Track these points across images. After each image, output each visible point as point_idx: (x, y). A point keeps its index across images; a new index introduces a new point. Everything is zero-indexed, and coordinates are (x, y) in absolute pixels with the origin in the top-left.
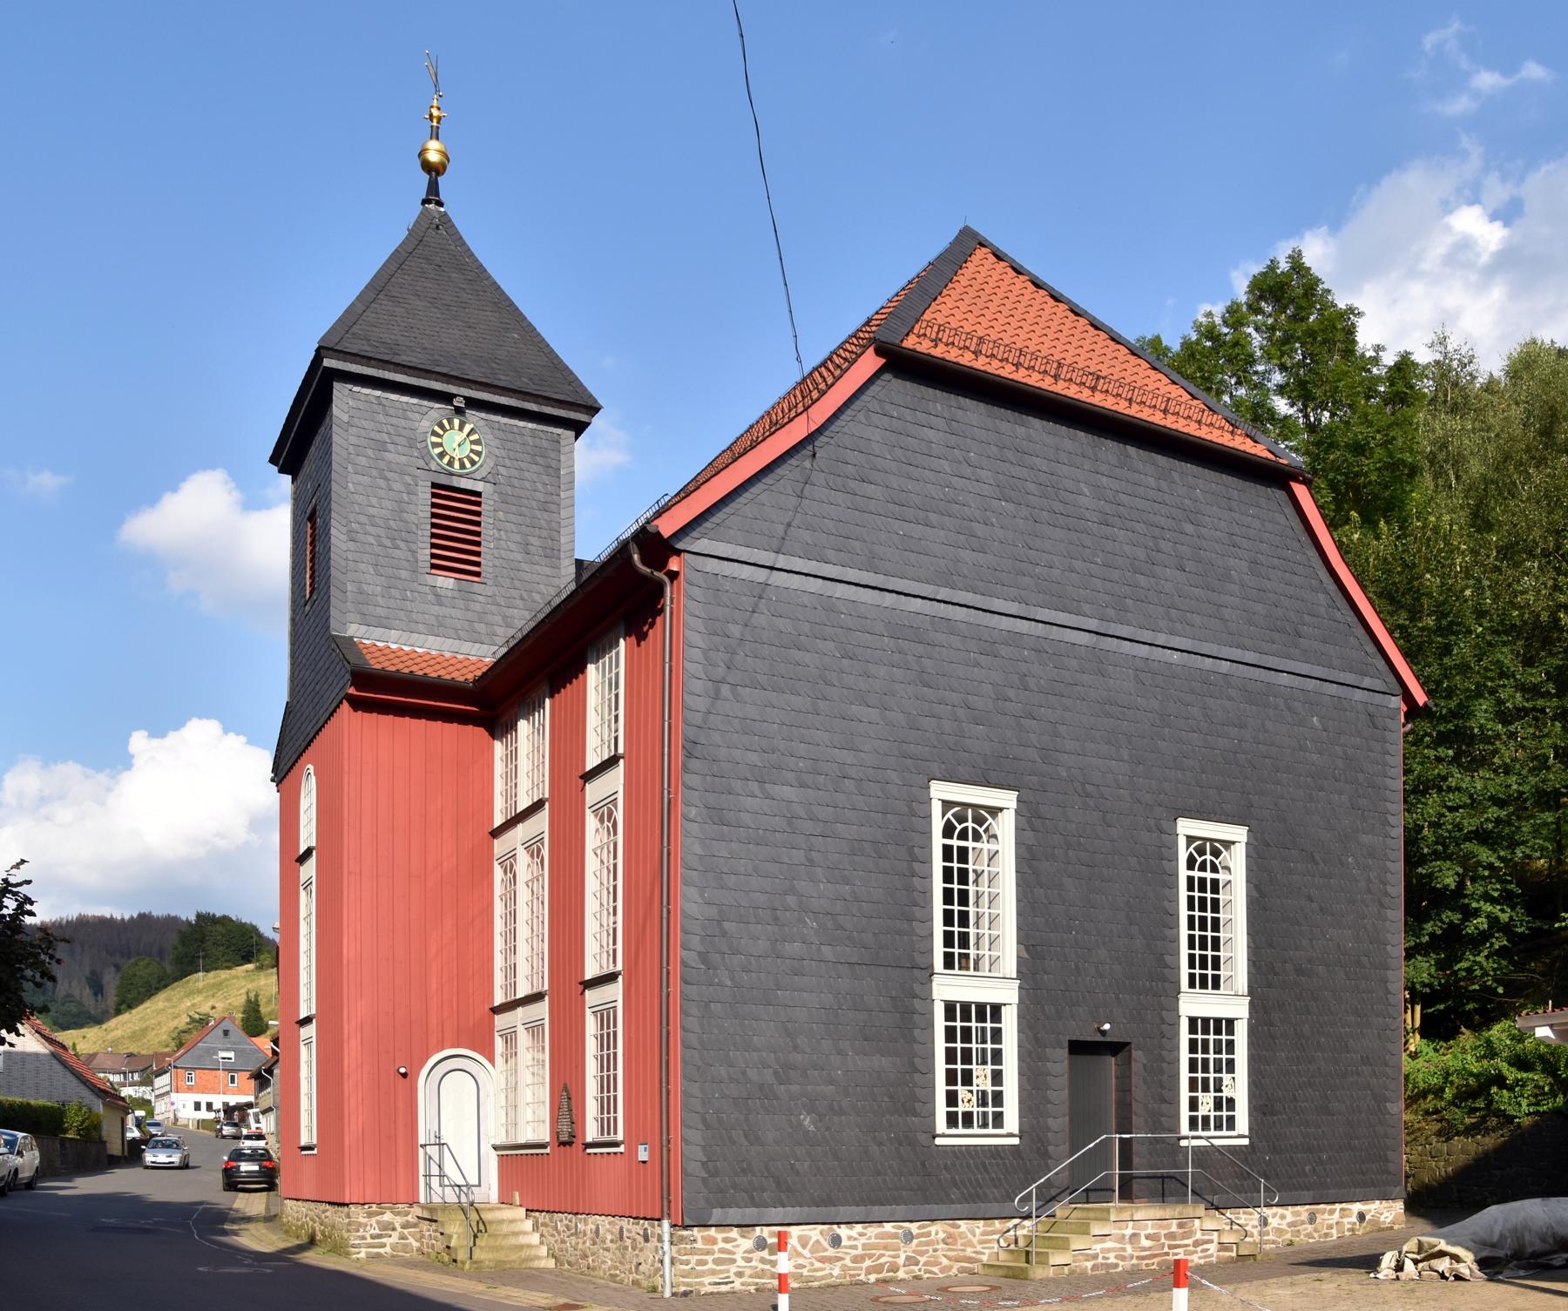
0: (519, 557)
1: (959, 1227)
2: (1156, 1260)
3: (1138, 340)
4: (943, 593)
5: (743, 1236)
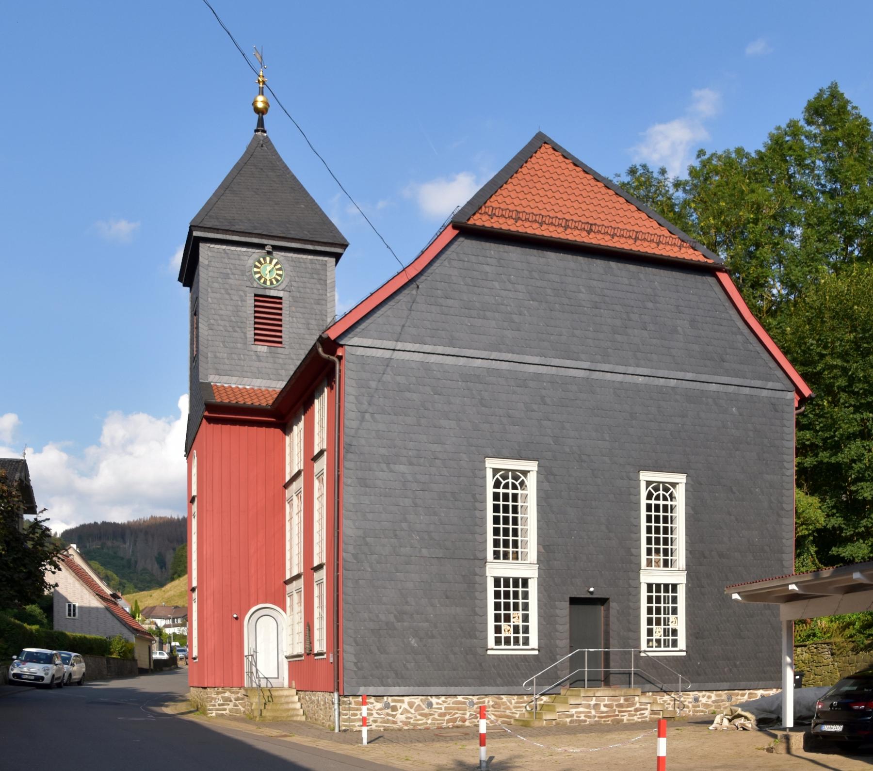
0: (303, 331)
1: (502, 699)
2: (610, 719)
3: (725, 152)
4: (494, 355)
5: (377, 702)
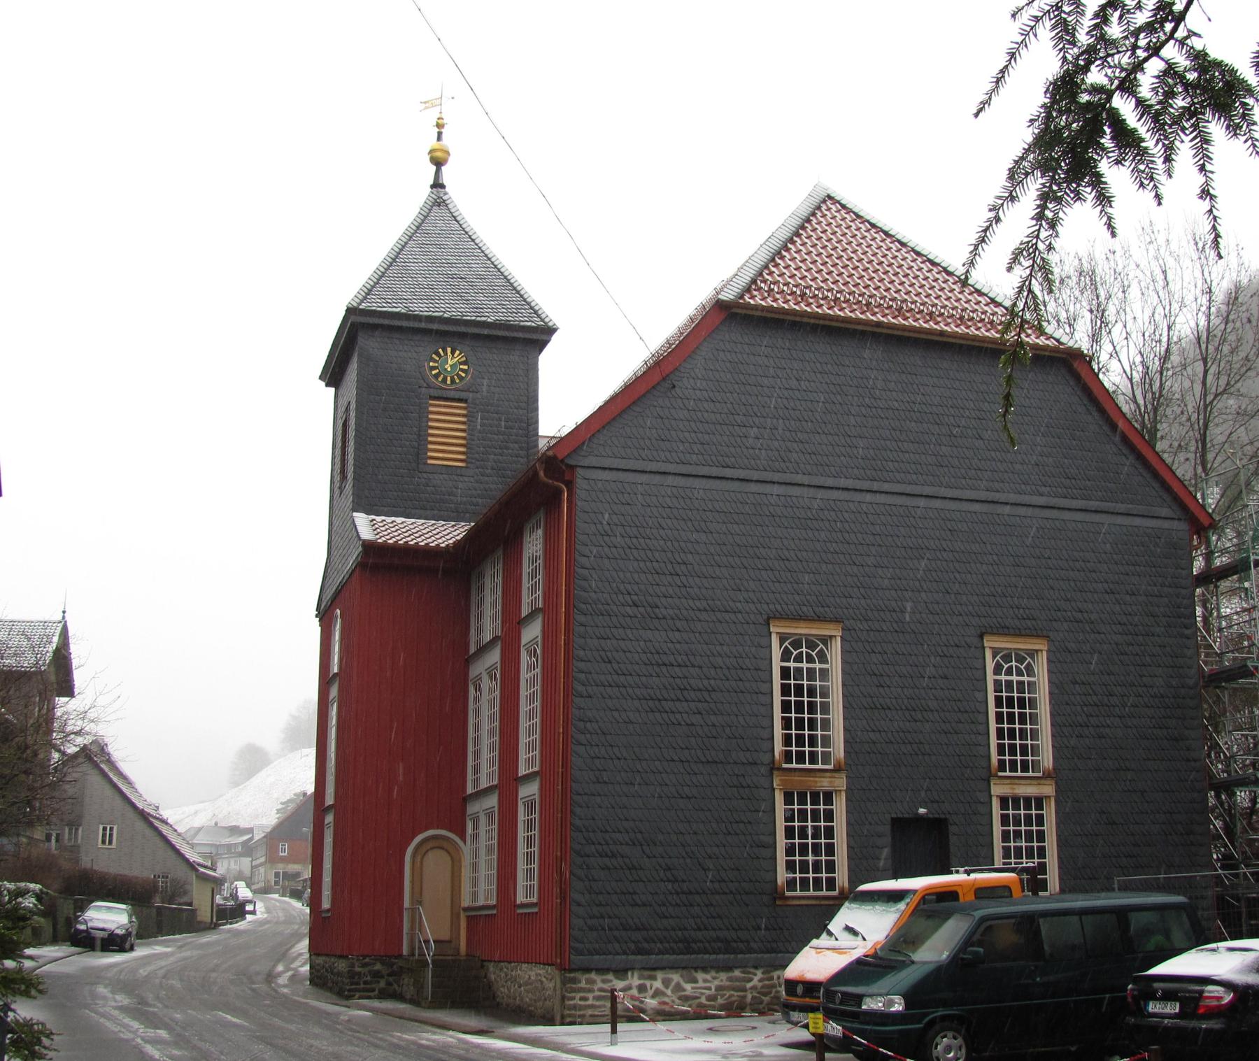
5: (617, 978)
